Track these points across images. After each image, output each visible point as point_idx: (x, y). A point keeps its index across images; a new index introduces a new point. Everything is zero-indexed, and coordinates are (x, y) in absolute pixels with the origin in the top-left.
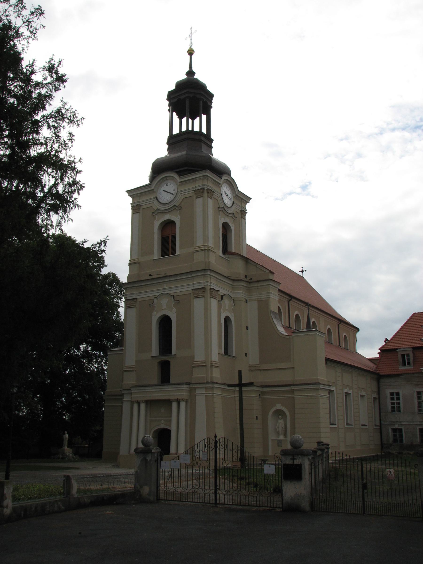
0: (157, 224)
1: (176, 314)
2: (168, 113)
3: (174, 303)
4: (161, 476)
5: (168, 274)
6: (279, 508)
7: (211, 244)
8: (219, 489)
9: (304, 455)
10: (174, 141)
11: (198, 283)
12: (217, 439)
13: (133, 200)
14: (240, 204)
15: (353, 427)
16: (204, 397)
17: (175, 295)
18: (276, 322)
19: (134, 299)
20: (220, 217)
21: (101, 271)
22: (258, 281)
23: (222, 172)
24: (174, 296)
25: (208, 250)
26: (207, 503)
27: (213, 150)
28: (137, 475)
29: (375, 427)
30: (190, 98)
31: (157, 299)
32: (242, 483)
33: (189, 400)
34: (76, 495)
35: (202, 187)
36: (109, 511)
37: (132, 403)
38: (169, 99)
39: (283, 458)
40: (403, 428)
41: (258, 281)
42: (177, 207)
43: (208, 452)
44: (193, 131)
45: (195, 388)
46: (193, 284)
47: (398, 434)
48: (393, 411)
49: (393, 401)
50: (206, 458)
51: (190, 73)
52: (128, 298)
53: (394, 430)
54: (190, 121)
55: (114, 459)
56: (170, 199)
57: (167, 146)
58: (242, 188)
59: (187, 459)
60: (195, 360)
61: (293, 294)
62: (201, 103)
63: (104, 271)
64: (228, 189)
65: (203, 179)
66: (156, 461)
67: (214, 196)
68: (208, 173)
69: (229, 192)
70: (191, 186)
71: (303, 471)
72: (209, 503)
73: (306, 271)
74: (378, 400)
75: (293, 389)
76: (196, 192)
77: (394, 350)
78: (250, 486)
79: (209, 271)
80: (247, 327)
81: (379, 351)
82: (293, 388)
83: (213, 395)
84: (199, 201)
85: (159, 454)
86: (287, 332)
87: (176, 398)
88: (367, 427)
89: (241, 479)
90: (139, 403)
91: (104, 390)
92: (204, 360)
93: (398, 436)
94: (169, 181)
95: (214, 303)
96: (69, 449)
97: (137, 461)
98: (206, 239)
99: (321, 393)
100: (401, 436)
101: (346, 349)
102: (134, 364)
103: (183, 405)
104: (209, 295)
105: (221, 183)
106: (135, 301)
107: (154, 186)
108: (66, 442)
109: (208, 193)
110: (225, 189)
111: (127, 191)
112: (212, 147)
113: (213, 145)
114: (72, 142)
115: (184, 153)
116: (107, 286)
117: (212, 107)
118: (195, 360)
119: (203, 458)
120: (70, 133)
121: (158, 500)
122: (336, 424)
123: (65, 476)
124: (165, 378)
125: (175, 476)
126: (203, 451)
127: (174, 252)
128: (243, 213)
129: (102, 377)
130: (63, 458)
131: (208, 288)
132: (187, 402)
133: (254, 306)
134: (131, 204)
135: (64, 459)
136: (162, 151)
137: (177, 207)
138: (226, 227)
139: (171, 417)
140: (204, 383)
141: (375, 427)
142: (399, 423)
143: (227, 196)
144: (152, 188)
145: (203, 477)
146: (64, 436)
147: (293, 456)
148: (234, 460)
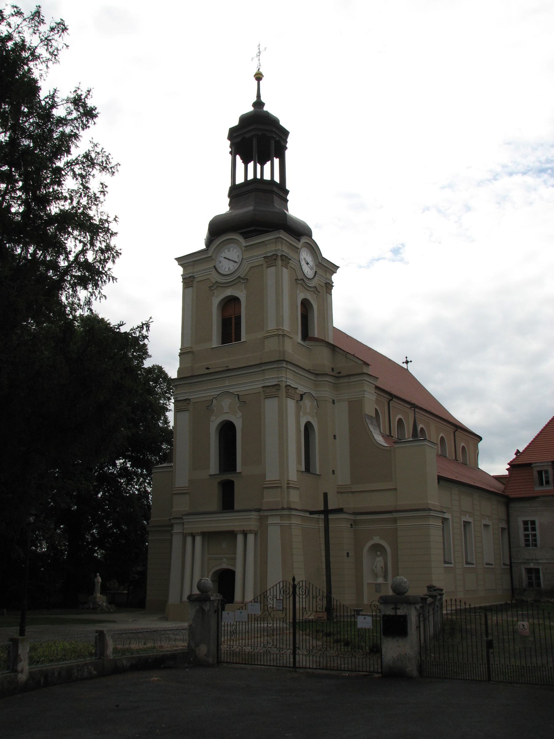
0: (216, 301)
2: (230, 157)
4: (223, 631)
6: (378, 673)
7: (286, 327)
10: (237, 193)
11: (270, 378)
12: (296, 583)
13: (184, 271)
17: (240, 394)
18: (372, 429)
20: (298, 292)
22: (349, 376)
23: (300, 233)
25: (283, 336)
30: (259, 136)
32: (328, 640)
34: (112, 657)
35: (274, 253)
36: (155, 677)
37: (185, 536)
38: (230, 137)
39: (382, 607)
40: (540, 567)
41: (349, 376)
42: (242, 279)
43: (285, 600)
45: (267, 516)
46: (263, 380)
47: (533, 576)
48: (527, 545)
49: (527, 533)
50: (281, 608)
51: (259, 104)
53: (529, 571)
54: (259, 166)
55: (161, 609)
58: (327, 253)
59: (256, 609)
60: (267, 479)
61: (394, 392)
62: (273, 143)
63: (148, 364)
64: (309, 255)
66: (216, 611)
68: (283, 235)
69: (309, 259)
70: (260, 252)
71: (409, 626)
73: (411, 361)
74: (508, 530)
76: (266, 260)
79: (284, 362)
80: (335, 436)
81: (508, 467)
82: (396, 515)
86: (386, 442)
87: (242, 529)
89: (328, 635)
90: (193, 536)
92: (278, 479)
93: (534, 578)
94: (232, 245)
95: (291, 404)
97: (191, 611)
98: (279, 320)
99: (432, 522)
100: (538, 578)
101: (464, 464)
102: (187, 485)
103: (251, 538)
104: (284, 394)
105: (299, 247)
108: (98, 588)
109: (282, 260)
110: (305, 256)
111: (176, 259)
112: (287, 201)
113: (289, 197)
115: (251, 208)
116: (151, 383)
117: (286, 148)
121: (219, 662)
122: (453, 562)
123: (97, 632)
124: (228, 502)
125: (241, 631)
126: (278, 598)
127: (238, 338)
128: (329, 286)
130: (93, 609)
131: (283, 385)
132: (256, 534)
135: (96, 609)
137: (242, 279)
138: (306, 304)
141: (503, 567)
143: (308, 264)
144: (209, 255)
146: (96, 579)
148: (318, 610)
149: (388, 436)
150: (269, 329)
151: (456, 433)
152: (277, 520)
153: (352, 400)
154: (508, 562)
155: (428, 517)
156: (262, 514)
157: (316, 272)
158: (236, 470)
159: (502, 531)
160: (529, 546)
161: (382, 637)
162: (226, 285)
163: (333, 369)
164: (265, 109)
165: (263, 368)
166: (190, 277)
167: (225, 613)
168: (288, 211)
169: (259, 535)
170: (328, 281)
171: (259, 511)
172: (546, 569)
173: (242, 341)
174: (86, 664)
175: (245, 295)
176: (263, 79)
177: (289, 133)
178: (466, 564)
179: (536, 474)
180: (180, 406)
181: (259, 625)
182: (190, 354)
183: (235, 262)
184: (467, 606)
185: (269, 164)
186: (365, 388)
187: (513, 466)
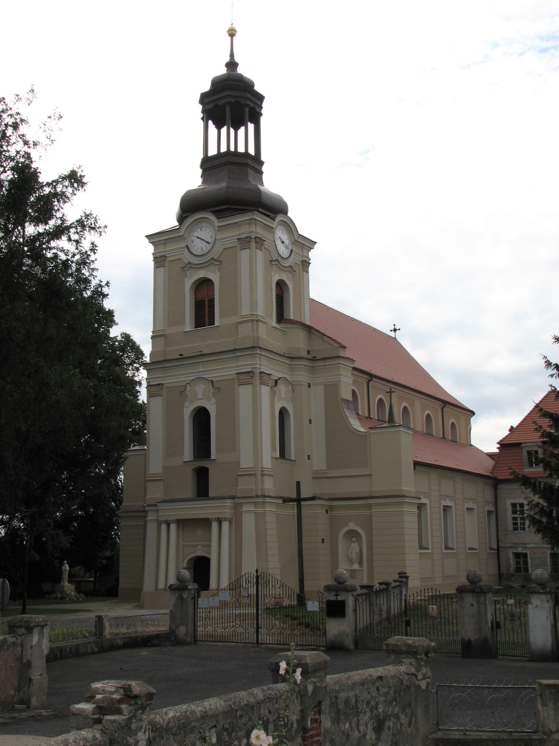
0: (189, 282)
1: (215, 405)
2: (201, 123)
3: (212, 391)
4: (199, 617)
5: (205, 352)
6: (323, 646)
7: (260, 312)
8: (261, 628)
9: (348, 591)
10: (210, 165)
12: (259, 574)
13: (155, 249)
14: (300, 253)
15: (455, 551)
16: (253, 515)
17: (214, 379)
18: (348, 414)
19: (159, 384)
20: (273, 273)
21: (109, 332)
22: (325, 359)
23: (275, 209)
24: (212, 381)
25: (257, 321)
26: (248, 643)
27: (265, 177)
28: (172, 614)
29: (489, 551)
30: (232, 101)
31: (190, 385)
32: (293, 623)
33: (234, 520)
35: (248, 235)
36: (144, 652)
39: (326, 594)
40: (528, 552)
41: (325, 359)
42: (215, 260)
43: (249, 588)
44: (236, 153)
45: (241, 504)
46: (238, 366)
47: (521, 560)
48: (515, 529)
49: (515, 516)
50: (247, 595)
51: (232, 65)
52: (151, 384)
53: (517, 555)
54: (232, 131)
55: (135, 596)
56: (205, 250)
57: (201, 171)
59: (226, 596)
60: (241, 467)
61: (374, 372)
62: (247, 110)
64: (284, 233)
65: (249, 224)
66: (193, 598)
67: (265, 246)
70: (233, 234)
71: (347, 608)
72: (251, 643)
73: (399, 329)
74: (495, 513)
75: (371, 502)
76: (240, 242)
77: (518, 445)
78: (301, 626)
79: (258, 349)
81: (499, 446)
82: (370, 501)
83: (264, 513)
84: (245, 254)
85: (196, 591)
86: (362, 426)
87: (217, 517)
88: (477, 551)
89: (294, 619)
90: (168, 524)
91: (119, 501)
92: (252, 466)
93: (522, 563)
94: (204, 224)
95: (265, 391)
96: (70, 585)
97: (171, 598)
98: (253, 305)
99: (406, 508)
100: (526, 563)
101: (454, 441)
102: (161, 472)
105: (274, 226)
106: (161, 387)
107: (183, 230)
108: (66, 576)
109: (256, 242)
110: (281, 234)
111: (146, 236)
112: (261, 173)
113: (264, 169)
114: (95, 253)
115: (224, 185)
116: (118, 352)
117: (261, 114)
118: (241, 467)
119: (244, 595)
120: (93, 244)
121: (196, 641)
122: (430, 548)
123: (96, 617)
124: (202, 490)
125: (216, 617)
126: (244, 586)
127: (212, 322)
128: (306, 264)
129: (113, 482)
130: (61, 598)
131: (257, 372)
132: (230, 522)
133: (318, 393)
134: (153, 254)
135: (63, 599)
136: (194, 180)
137: (215, 260)
138: (281, 286)
139: (210, 541)
140: (252, 497)
141: (489, 551)
142: (524, 546)
143: (283, 242)
144: (181, 234)
145: (250, 618)
146: (63, 567)
147: (337, 592)
148: (277, 596)
149: (367, 418)
150: (243, 314)
151: (444, 409)
152: (252, 508)
153: (330, 383)
154: (495, 546)
155: (402, 503)
156: (237, 502)
157: (292, 250)
158: (210, 457)
159: (488, 514)
160: (518, 530)
161: (326, 617)
162: (200, 267)
163: (308, 351)
164: (240, 70)
165: (237, 355)
166: (162, 256)
167: (200, 600)
168: (262, 184)
169: (234, 522)
170: (305, 259)
171: (233, 499)
172: (534, 554)
173: (216, 325)
174: (89, 642)
175: (218, 278)
176: (237, 34)
177: (264, 97)
178: (446, 549)
179: (525, 454)
180: (154, 391)
181: (231, 612)
182: (163, 338)
183: (208, 243)
184: (438, 593)
185: (242, 129)
186: (342, 372)
187: (503, 445)
